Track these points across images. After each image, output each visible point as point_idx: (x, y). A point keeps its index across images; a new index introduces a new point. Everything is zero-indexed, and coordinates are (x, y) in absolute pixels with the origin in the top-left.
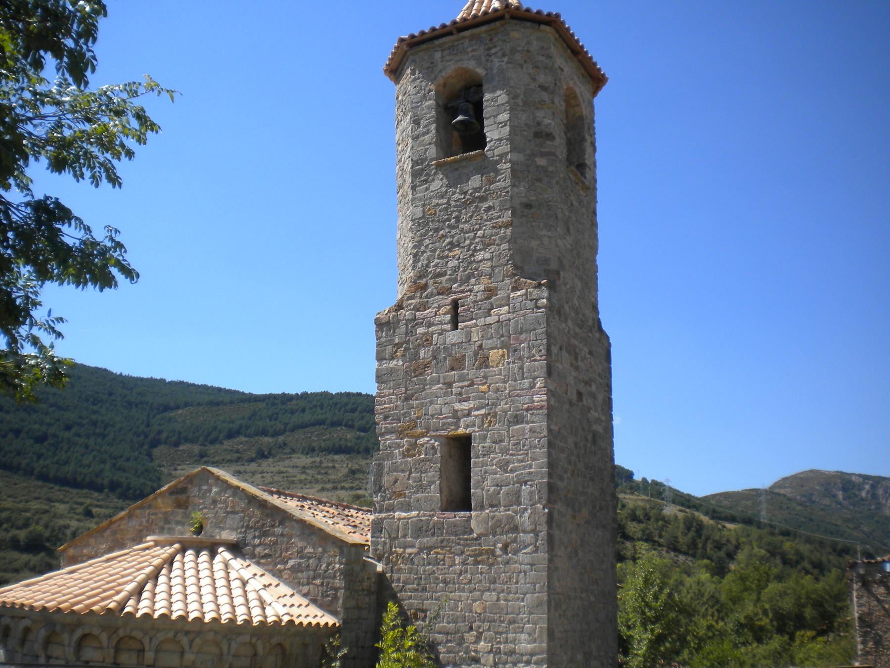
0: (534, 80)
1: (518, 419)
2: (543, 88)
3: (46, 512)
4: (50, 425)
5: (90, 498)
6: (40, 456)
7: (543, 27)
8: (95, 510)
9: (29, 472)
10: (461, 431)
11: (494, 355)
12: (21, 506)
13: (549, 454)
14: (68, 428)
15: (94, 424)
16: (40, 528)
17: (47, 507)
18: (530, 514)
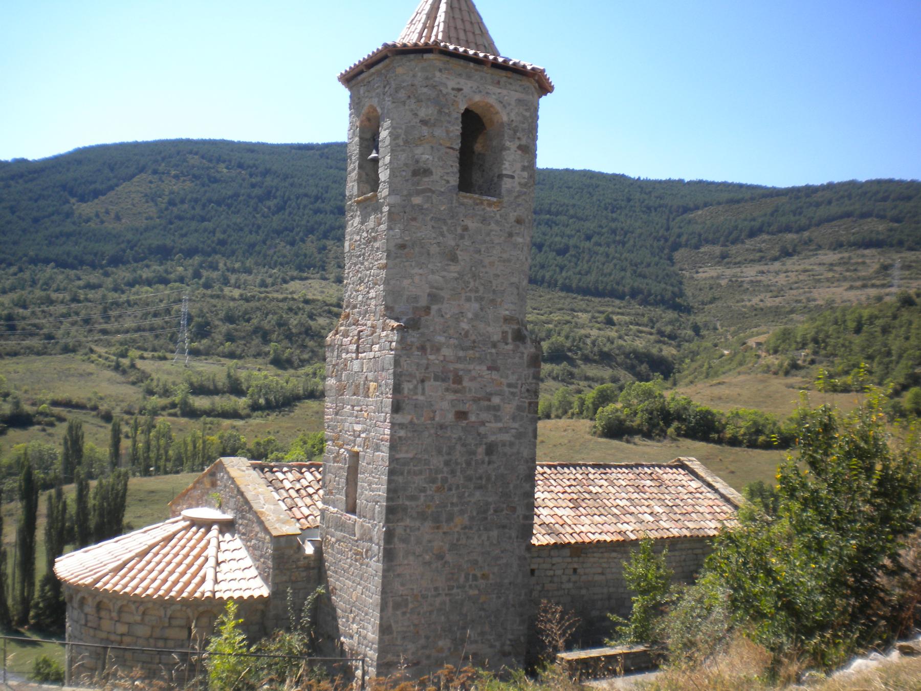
0: (416, 115)
1: (377, 448)
2: (424, 122)
3: (568, 322)
4: (570, 237)
5: (612, 306)
6: (562, 268)
7: (426, 56)
8: (615, 318)
9: (552, 284)
10: (356, 449)
11: (373, 385)
12: (543, 318)
13: (390, 482)
14: (588, 238)
15: (614, 232)
16: (561, 339)
17: (569, 318)
18: (378, 530)
